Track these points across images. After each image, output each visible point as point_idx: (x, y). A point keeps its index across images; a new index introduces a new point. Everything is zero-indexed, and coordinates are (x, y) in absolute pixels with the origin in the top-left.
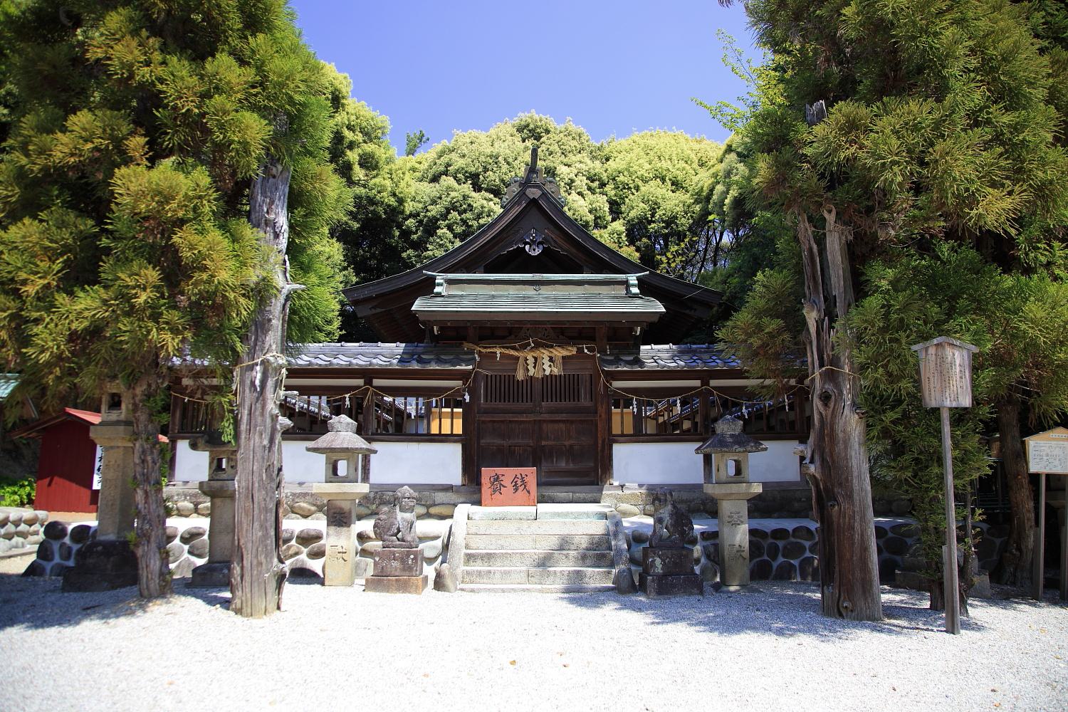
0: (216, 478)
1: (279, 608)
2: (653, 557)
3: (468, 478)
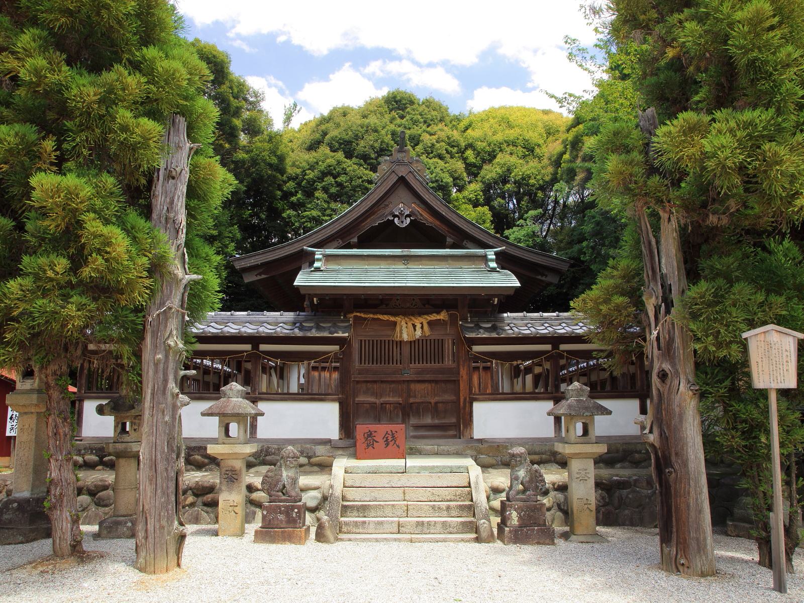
0: (120, 440)
1: (179, 565)
2: (510, 511)
3: (345, 432)
